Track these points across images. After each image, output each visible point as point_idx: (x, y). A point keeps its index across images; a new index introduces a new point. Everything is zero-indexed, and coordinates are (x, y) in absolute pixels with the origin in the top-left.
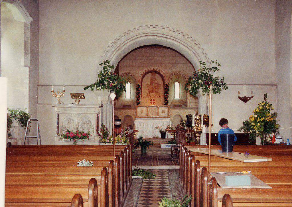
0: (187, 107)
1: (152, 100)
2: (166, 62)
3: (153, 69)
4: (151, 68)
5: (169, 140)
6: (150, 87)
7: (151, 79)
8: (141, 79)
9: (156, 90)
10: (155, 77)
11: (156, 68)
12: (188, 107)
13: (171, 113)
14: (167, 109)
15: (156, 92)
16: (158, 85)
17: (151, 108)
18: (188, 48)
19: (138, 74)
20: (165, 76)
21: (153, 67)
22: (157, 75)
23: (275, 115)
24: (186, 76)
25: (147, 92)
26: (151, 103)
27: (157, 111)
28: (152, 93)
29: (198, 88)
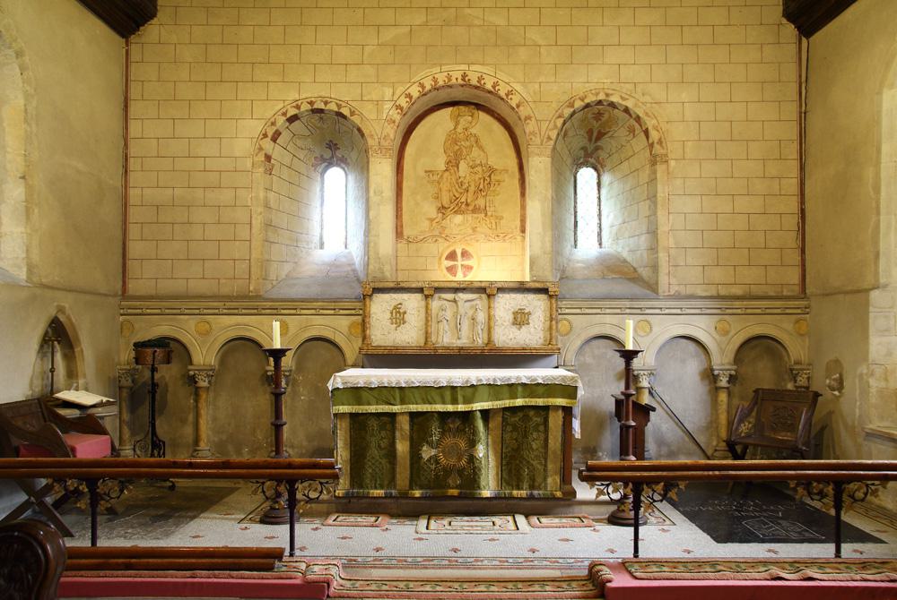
0: (657, 293)
1: (451, 263)
2: (534, 35)
3: (464, 76)
4: (450, 72)
5: (827, 394)
6: (445, 186)
7: (452, 140)
8: (392, 136)
9: (481, 202)
10: (473, 131)
11: (487, 73)
12: (663, 280)
13: (563, 326)
14: (539, 303)
15: (476, 210)
16: (492, 171)
17: (450, 296)
18: (206, 297)
19: (378, 103)
20: (528, 118)
21: (464, 67)
22: (483, 116)
23: (830, 413)
24: (647, 114)
25: (431, 210)
26: (451, 270)
27: (481, 317)
28: (458, 219)
29: (29, 490)
